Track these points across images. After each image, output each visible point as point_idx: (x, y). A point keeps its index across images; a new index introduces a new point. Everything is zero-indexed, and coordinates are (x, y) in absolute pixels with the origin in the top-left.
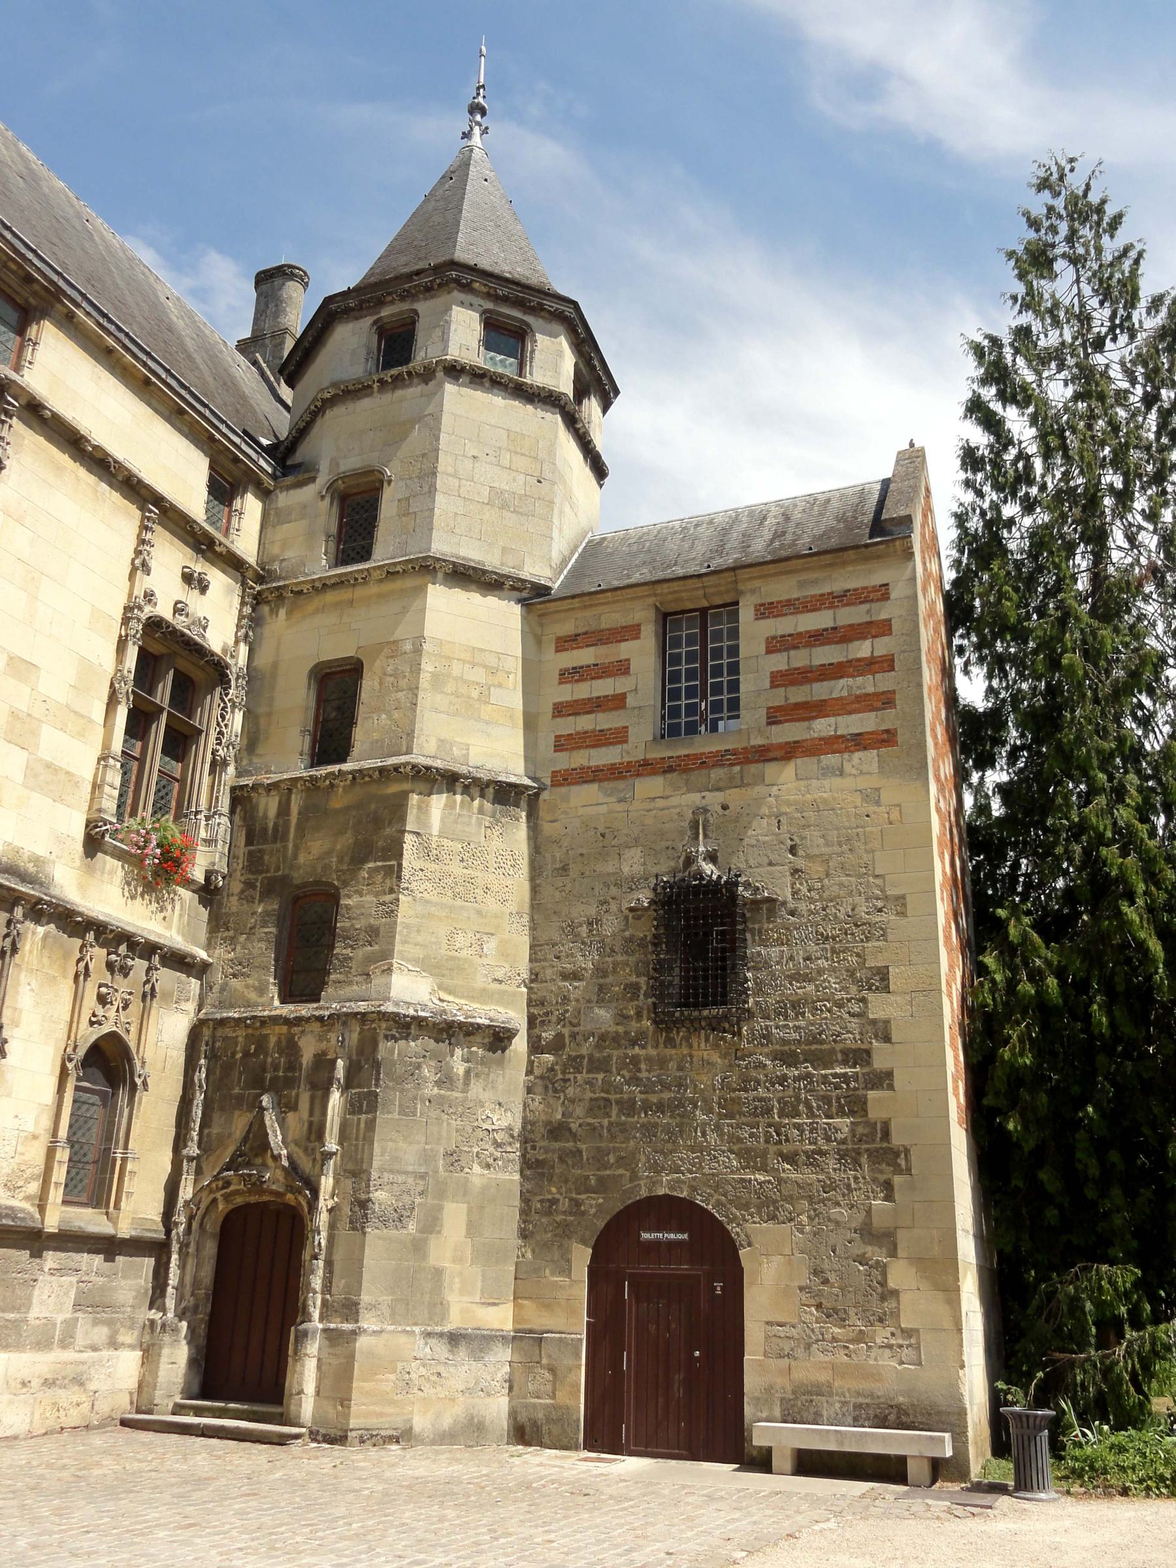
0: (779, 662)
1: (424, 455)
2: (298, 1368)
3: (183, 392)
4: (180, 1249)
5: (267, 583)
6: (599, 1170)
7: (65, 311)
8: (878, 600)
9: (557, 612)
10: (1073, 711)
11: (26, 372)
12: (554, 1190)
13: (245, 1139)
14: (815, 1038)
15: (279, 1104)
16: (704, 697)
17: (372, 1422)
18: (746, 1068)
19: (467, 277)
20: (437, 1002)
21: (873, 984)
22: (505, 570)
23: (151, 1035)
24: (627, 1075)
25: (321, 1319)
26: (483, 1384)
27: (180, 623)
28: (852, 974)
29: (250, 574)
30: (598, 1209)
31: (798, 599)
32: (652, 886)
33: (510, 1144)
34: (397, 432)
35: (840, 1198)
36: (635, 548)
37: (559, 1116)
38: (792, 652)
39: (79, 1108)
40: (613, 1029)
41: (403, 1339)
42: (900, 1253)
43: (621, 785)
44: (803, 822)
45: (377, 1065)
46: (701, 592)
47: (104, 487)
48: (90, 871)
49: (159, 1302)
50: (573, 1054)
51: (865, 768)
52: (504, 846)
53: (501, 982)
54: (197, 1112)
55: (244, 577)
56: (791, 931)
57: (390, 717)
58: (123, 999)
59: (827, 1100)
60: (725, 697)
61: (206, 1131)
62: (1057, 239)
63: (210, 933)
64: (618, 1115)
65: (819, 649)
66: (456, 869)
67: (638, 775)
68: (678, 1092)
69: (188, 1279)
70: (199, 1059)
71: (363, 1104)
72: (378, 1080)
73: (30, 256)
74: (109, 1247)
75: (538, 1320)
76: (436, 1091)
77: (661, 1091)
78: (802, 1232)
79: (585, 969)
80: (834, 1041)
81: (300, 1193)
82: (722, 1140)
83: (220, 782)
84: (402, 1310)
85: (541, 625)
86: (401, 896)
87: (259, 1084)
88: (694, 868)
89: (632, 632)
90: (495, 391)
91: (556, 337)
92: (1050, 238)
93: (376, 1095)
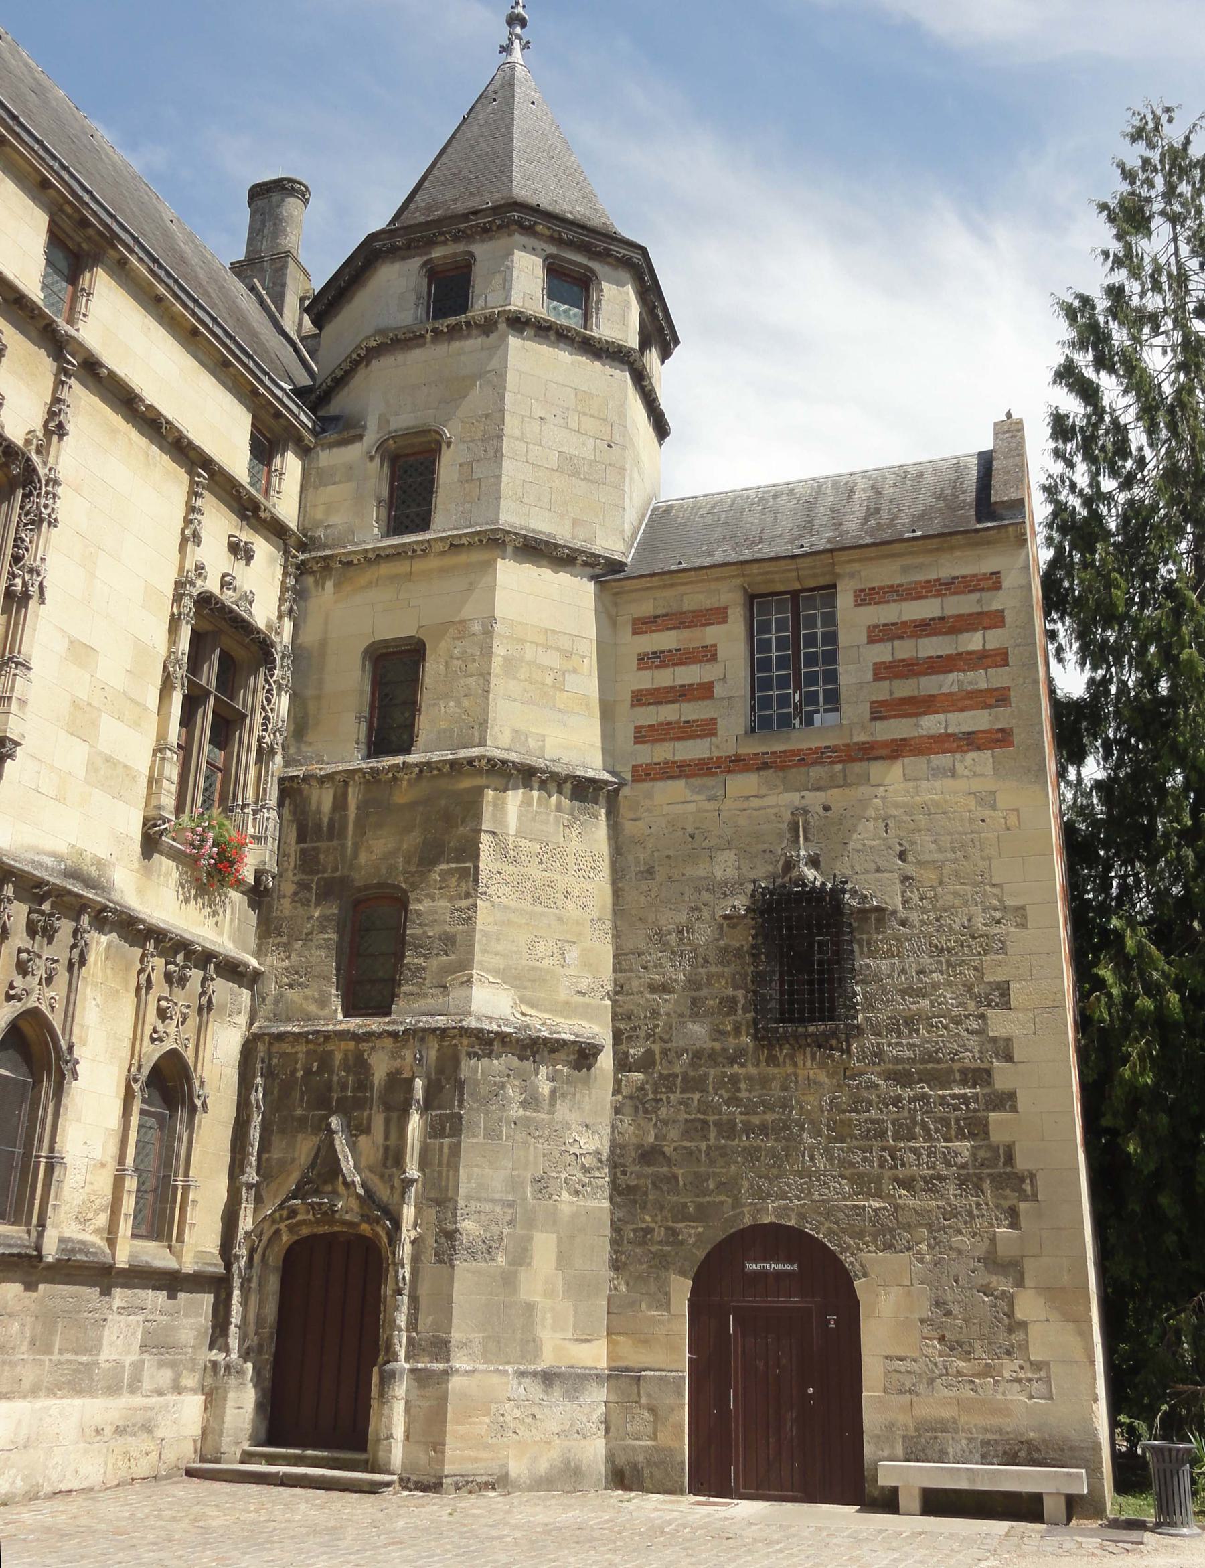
0: (883, 653)
1: (487, 416)
2: (386, 1411)
3: (228, 342)
4: (242, 1285)
5: (310, 551)
6: (697, 1196)
7: (117, 256)
8: (989, 589)
9: (636, 590)
10: (1187, 709)
11: (80, 325)
12: (648, 1218)
13: (313, 1165)
14: (930, 1056)
15: (349, 1126)
16: (798, 687)
17: (468, 1467)
18: (857, 1088)
19: (530, 219)
20: (519, 1016)
21: (992, 1000)
22: (577, 544)
23: (207, 1053)
24: (726, 1096)
25: (407, 1359)
26: (579, 1426)
27: (228, 597)
28: (969, 988)
29: (292, 541)
30: (698, 1238)
31: (902, 585)
32: (749, 893)
33: (598, 1169)
34: (456, 388)
35: (962, 1226)
36: (709, 518)
37: (651, 1139)
38: (896, 643)
39: (145, 1134)
40: (709, 1045)
41: (495, 1379)
42: (1028, 1283)
43: (710, 781)
44: (913, 826)
45: (460, 1085)
46: (794, 574)
47: (155, 449)
48: (147, 872)
49: (220, 1341)
50: (665, 1072)
51: (978, 769)
52: (583, 847)
53: (584, 994)
54: (255, 1135)
55: (285, 544)
56: (902, 943)
57: (458, 703)
58: (182, 1013)
59: (945, 1122)
60: (820, 688)
61: (265, 1156)
62: (1153, 194)
63: (260, 938)
64: (716, 1138)
65: (926, 640)
66: (535, 871)
67: (729, 772)
68: (783, 1113)
69: (252, 1316)
70: (254, 1077)
71: (446, 1127)
72: (461, 1101)
73: (86, 198)
74: (172, 1282)
75: (634, 1357)
76: (521, 1112)
77: (764, 1112)
78: (921, 1261)
79: (676, 981)
80: (952, 1060)
81: (378, 1223)
82: (832, 1164)
83: (267, 772)
84: (494, 1349)
85: (616, 604)
86: (478, 902)
87: (324, 1103)
88: (795, 873)
89: (718, 615)
90: (561, 345)
91: (623, 286)
92: (1144, 193)
93: (460, 1117)
